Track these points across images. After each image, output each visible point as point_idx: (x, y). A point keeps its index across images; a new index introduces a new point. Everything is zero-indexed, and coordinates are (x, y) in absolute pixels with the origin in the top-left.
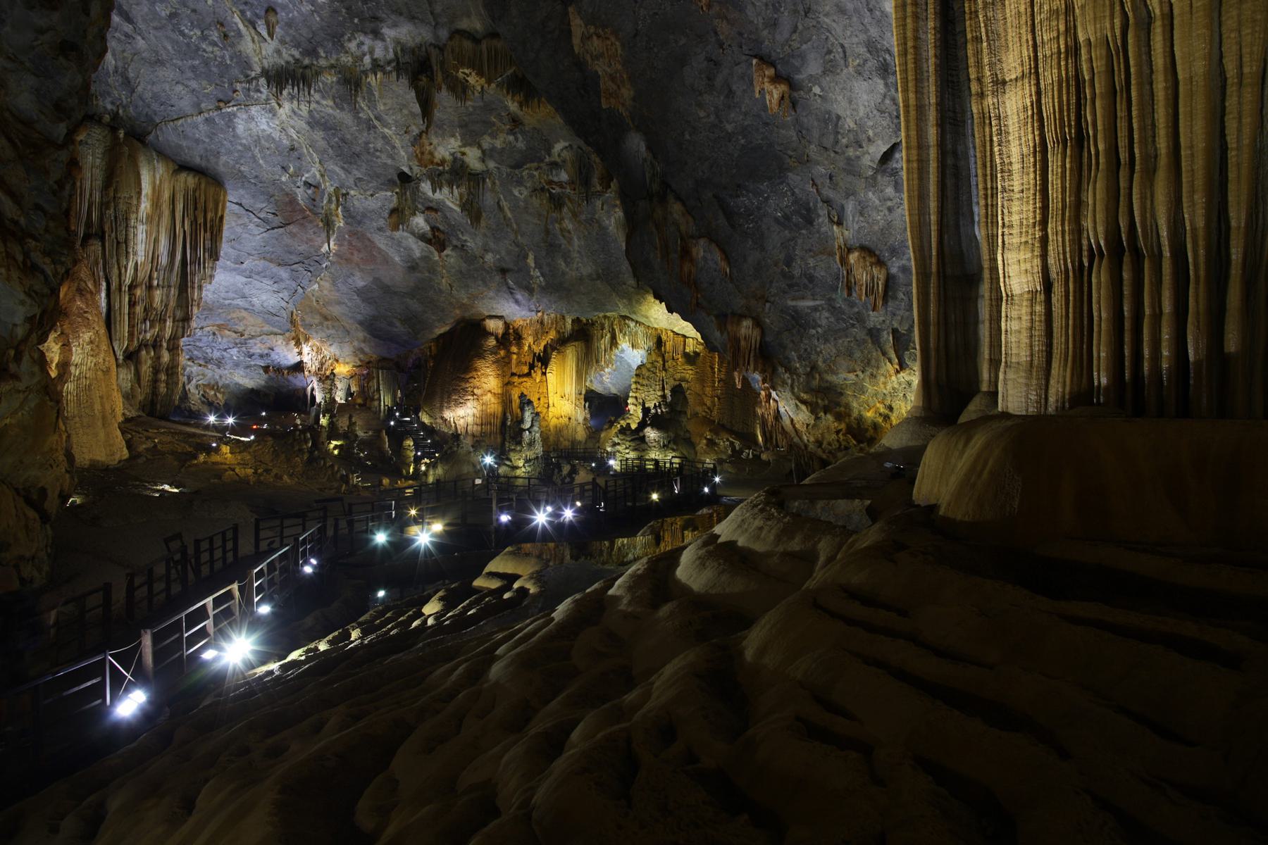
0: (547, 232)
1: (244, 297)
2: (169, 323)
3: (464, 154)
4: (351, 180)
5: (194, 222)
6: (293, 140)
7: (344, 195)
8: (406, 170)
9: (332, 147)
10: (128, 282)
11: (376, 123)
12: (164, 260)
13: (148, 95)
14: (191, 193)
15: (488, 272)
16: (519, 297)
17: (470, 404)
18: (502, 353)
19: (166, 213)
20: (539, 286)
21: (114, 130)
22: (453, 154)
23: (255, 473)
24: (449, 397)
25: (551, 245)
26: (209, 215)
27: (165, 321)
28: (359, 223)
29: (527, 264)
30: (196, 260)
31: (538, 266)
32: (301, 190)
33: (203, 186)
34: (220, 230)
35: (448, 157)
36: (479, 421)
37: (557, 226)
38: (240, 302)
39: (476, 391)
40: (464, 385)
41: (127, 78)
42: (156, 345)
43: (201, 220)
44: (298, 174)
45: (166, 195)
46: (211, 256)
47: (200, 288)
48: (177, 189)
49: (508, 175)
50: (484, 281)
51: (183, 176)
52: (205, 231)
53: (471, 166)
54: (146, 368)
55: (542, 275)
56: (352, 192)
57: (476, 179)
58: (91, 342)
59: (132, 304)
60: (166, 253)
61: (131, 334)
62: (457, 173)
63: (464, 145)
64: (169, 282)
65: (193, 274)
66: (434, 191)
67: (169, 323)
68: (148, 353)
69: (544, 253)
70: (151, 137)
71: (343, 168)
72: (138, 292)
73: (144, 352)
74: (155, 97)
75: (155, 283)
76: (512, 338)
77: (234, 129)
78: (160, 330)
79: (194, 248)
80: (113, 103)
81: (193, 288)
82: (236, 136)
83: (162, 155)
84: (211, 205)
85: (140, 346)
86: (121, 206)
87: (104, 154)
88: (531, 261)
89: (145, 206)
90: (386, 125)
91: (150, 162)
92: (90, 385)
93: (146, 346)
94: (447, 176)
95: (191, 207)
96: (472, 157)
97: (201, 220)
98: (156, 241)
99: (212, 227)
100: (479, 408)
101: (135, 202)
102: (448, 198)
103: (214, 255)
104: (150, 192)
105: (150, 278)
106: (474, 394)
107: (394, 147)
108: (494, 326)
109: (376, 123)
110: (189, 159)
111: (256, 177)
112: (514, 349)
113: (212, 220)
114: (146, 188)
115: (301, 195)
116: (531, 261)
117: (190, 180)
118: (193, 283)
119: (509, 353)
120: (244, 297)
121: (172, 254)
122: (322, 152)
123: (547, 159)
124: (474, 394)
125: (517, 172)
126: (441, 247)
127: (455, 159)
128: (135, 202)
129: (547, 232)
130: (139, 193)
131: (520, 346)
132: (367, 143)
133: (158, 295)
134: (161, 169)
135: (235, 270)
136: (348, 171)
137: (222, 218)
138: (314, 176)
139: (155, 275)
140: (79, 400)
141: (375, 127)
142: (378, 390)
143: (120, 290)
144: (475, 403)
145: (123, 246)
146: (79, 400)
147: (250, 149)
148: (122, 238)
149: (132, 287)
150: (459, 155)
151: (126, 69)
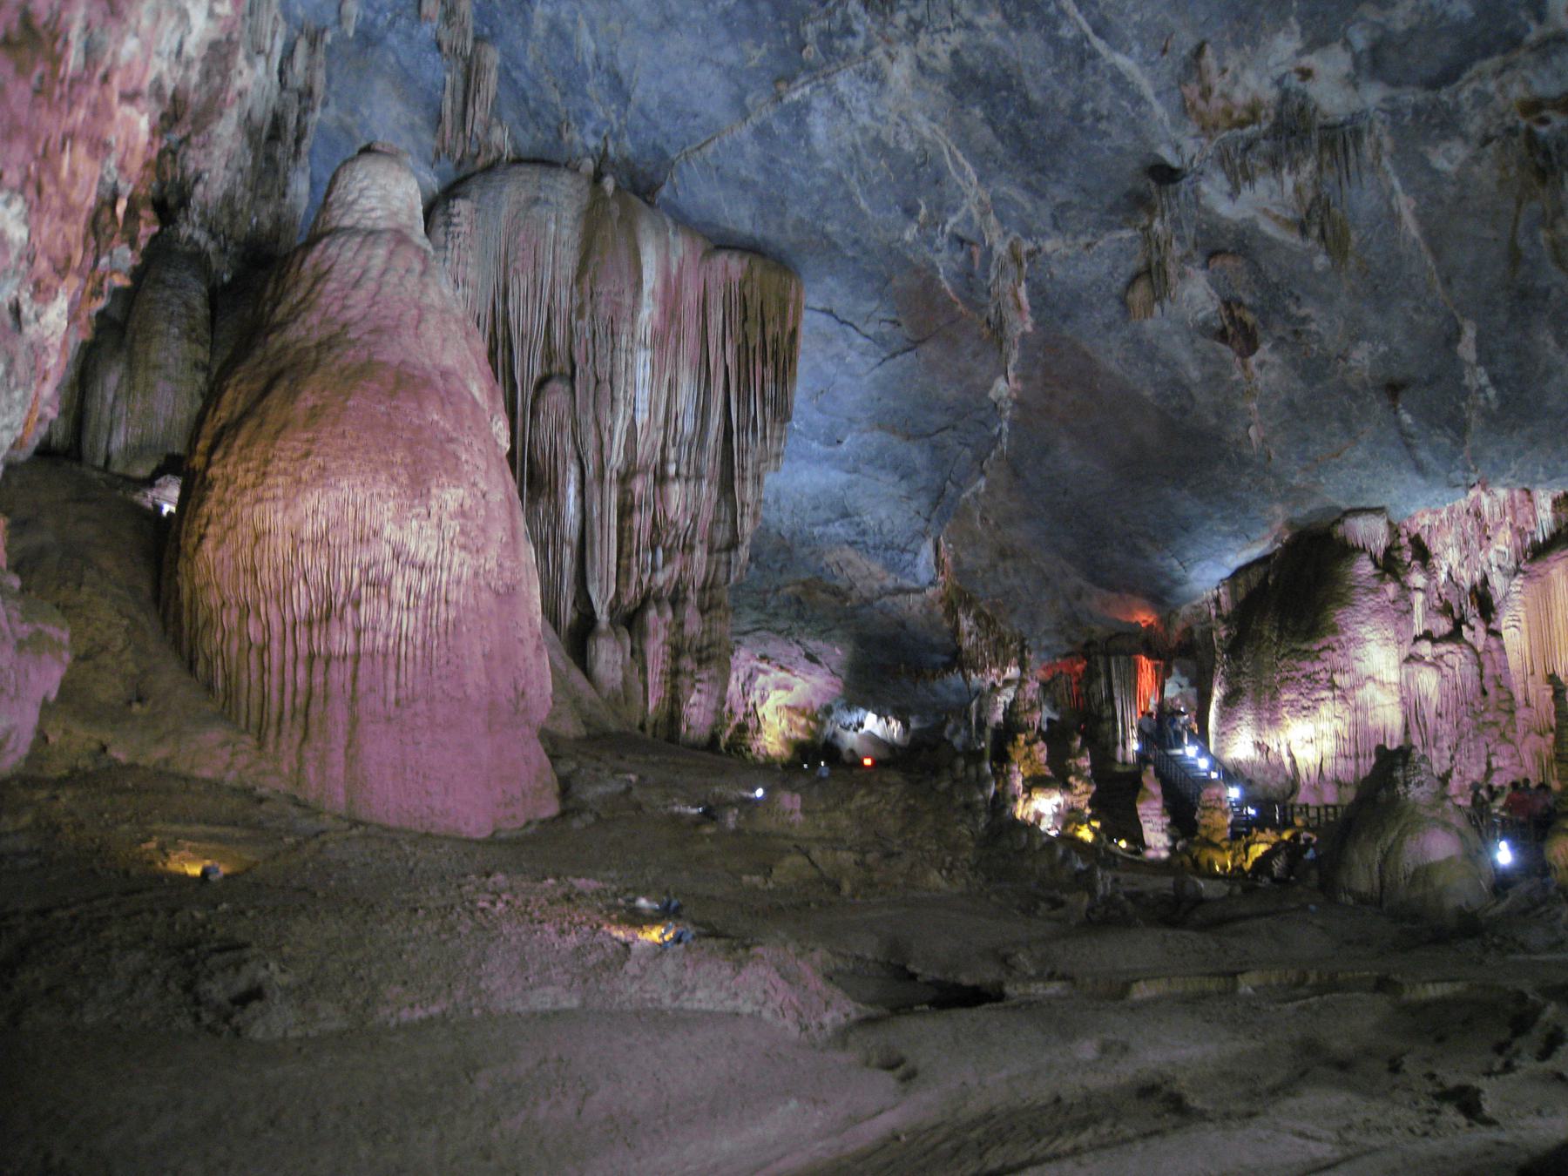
0: (1515, 257)
1: (845, 515)
2: (700, 554)
3: (1306, 74)
4: (1046, 212)
5: (744, 349)
6: (922, 140)
7: (1030, 254)
8: (1167, 154)
9: (1001, 138)
10: (616, 460)
11: (1099, 44)
12: (688, 425)
13: (653, 102)
14: (735, 289)
15: (1354, 395)
16: (1424, 454)
17: (1325, 710)
18: (1391, 589)
19: (692, 331)
20: (1485, 414)
21: (597, 178)
22: (1279, 82)
23: (860, 863)
24: (1273, 698)
25: (1523, 295)
26: (771, 330)
27: (692, 548)
28: (1065, 317)
29: (1456, 360)
30: (750, 425)
31: (1486, 357)
32: (944, 255)
33: (757, 274)
34: (791, 360)
35: (1270, 94)
36: (1349, 748)
37: (1543, 235)
38: (837, 529)
39: (1337, 678)
40: (1308, 667)
41: (617, 76)
42: (677, 599)
43: (755, 340)
44: (935, 221)
45: (691, 296)
46: (775, 414)
47: (758, 479)
48: (711, 284)
49: (1417, 111)
50: (1345, 420)
51: (722, 257)
52: (764, 363)
53: (1326, 106)
54: (656, 649)
55: (1495, 381)
56: (1048, 245)
57: (1339, 140)
58: (462, 513)
59: (625, 511)
60: (691, 410)
61: (623, 572)
62: (1293, 128)
63: (1309, 49)
64: (697, 469)
65: (744, 452)
66: (1234, 194)
67: (700, 554)
68: (660, 613)
69: (1502, 318)
70: (664, 192)
71: (1027, 186)
72: (638, 486)
73: (652, 614)
74: (666, 102)
75: (672, 469)
76: (1407, 556)
77: (808, 143)
78: (685, 568)
79: (744, 401)
80: (596, 133)
81: (743, 479)
82: (812, 157)
83: (683, 221)
84: (772, 309)
85: (645, 601)
86: (602, 308)
87: (576, 220)
88: (1467, 349)
89: (648, 313)
90: (1119, 45)
91: (660, 231)
92: (457, 623)
93: (658, 601)
94: (1264, 146)
95: (737, 317)
96: (1332, 90)
97: (755, 340)
98: (673, 386)
99: (775, 353)
100: (1348, 718)
101: (627, 300)
102: (1261, 203)
103: (782, 411)
104: (659, 286)
105: (664, 461)
106: (1333, 686)
107: (1139, 100)
108: (1370, 532)
109: (1099, 44)
110: (731, 226)
111: (856, 242)
112: (1418, 579)
113: (776, 340)
114: (651, 278)
115: (945, 263)
116: (1467, 349)
117: (735, 265)
118: (744, 469)
119: (1406, 589)
120: (845, 515)
121: (703, 414)
122: (981, 159)
123: (1534, 33)
124: (1333, 686)
125: (1444, 95)
126: (1248, 341)
127: (1285, 97)
128: (627, 300)
129: (1515, 257)
130: (638, 285)
131: (1430, 572)
132: (1077, 105)
133: (675, 491)
134: (681, 247)
135: (827, 458)
136: (1037, 193)
137: (794, 334)
138: (969, 220)
139: (672, 454)
140: (427, 657)
141: (1094, 55)
142: (1111, 699)
143: (601, 477)
144: (1339, 707)
145: (605, 388)
146: (427, 657)
147: (840, 179)
148: (604, 372)
149: (625, 479)
150: (1294, 82)
151: (612, 54)
